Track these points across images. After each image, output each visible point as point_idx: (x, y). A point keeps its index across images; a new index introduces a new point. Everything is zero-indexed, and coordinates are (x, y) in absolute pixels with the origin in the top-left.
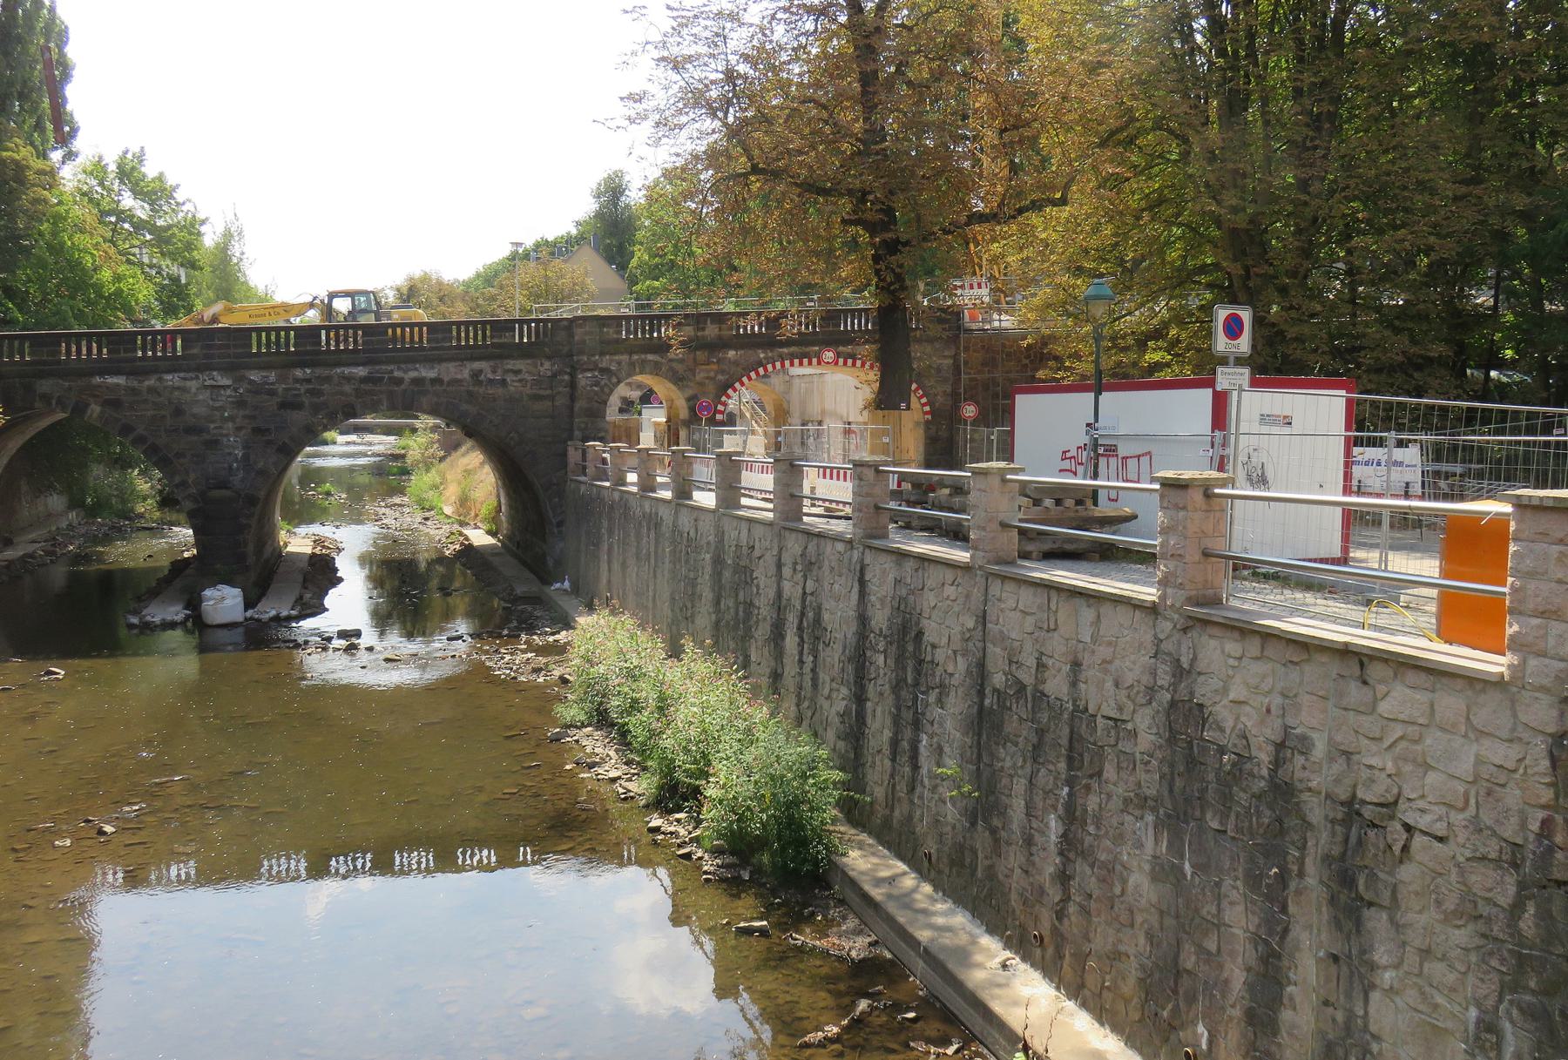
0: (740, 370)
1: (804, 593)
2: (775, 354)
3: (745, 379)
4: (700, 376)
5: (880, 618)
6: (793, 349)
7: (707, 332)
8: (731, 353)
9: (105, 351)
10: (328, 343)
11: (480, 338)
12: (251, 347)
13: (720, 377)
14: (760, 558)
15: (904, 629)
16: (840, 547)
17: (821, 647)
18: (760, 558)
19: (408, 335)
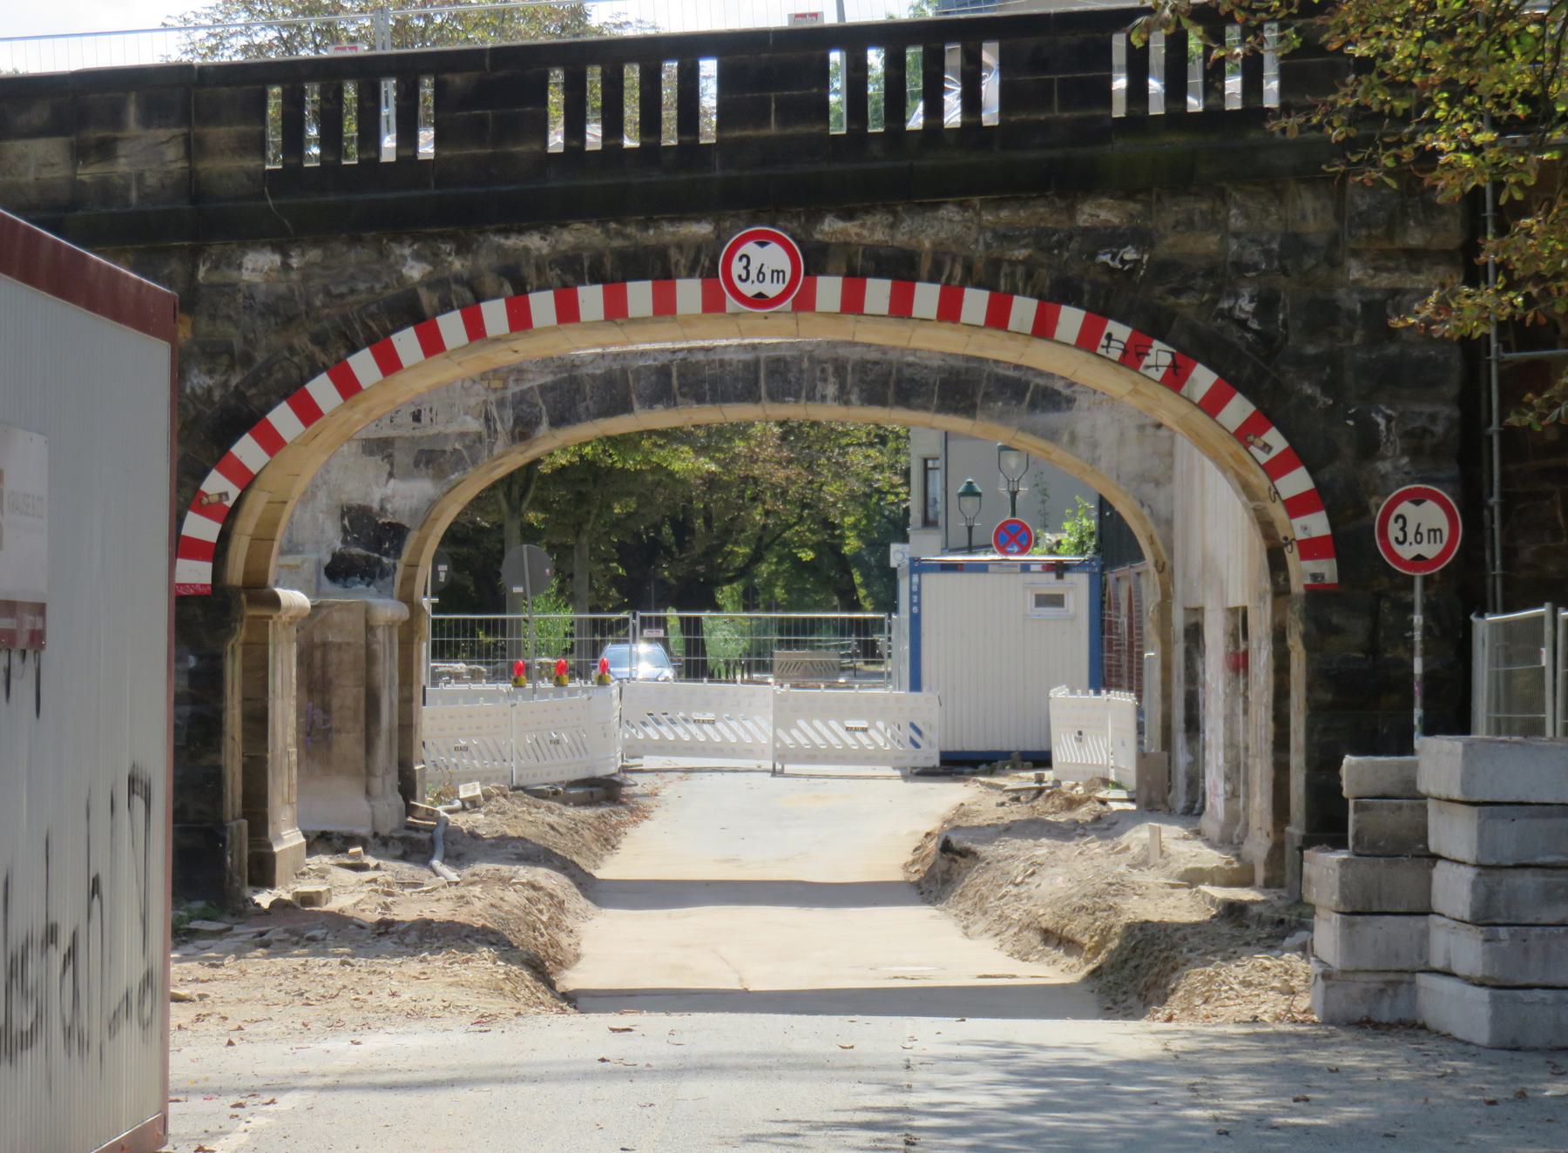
0: (302, 341)
2: (485, 261)
3: (321, 389)
6: (570, 237)
7: (122, 166)
10: (1138, 91)
11: (632, 111)
12: (543, 134)
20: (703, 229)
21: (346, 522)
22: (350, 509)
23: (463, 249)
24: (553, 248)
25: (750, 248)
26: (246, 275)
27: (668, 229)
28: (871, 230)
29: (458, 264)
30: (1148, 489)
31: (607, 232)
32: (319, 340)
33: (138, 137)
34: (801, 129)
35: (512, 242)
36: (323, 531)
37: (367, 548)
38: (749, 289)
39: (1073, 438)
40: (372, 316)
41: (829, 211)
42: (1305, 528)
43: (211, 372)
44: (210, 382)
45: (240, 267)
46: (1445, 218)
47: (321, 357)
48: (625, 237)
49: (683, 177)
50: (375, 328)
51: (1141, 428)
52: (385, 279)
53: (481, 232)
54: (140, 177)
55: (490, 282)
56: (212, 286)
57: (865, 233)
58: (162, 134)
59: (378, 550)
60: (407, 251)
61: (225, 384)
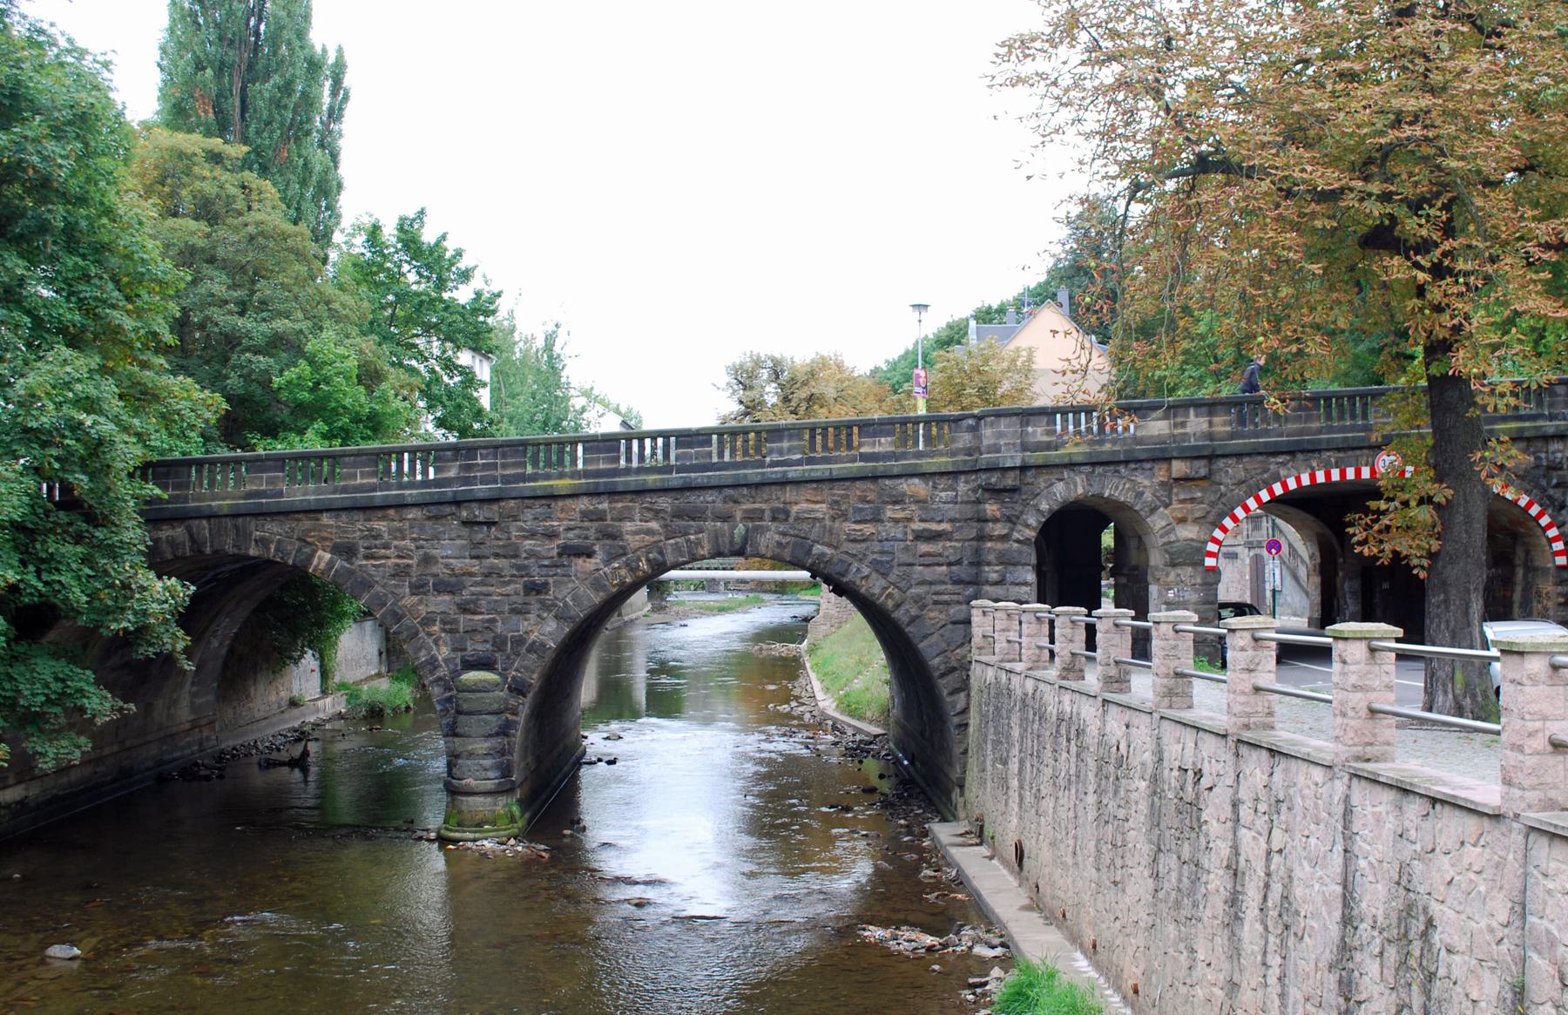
1: (1269, 853)
5: (1375, 900)
9: (431, 470)
14: (1210, 789)
15: (1409, 910)
16: (1318, 774)
17: (1291, 941)
18: (1210, 789)
19: (648, 451)
58: (1202, 420)
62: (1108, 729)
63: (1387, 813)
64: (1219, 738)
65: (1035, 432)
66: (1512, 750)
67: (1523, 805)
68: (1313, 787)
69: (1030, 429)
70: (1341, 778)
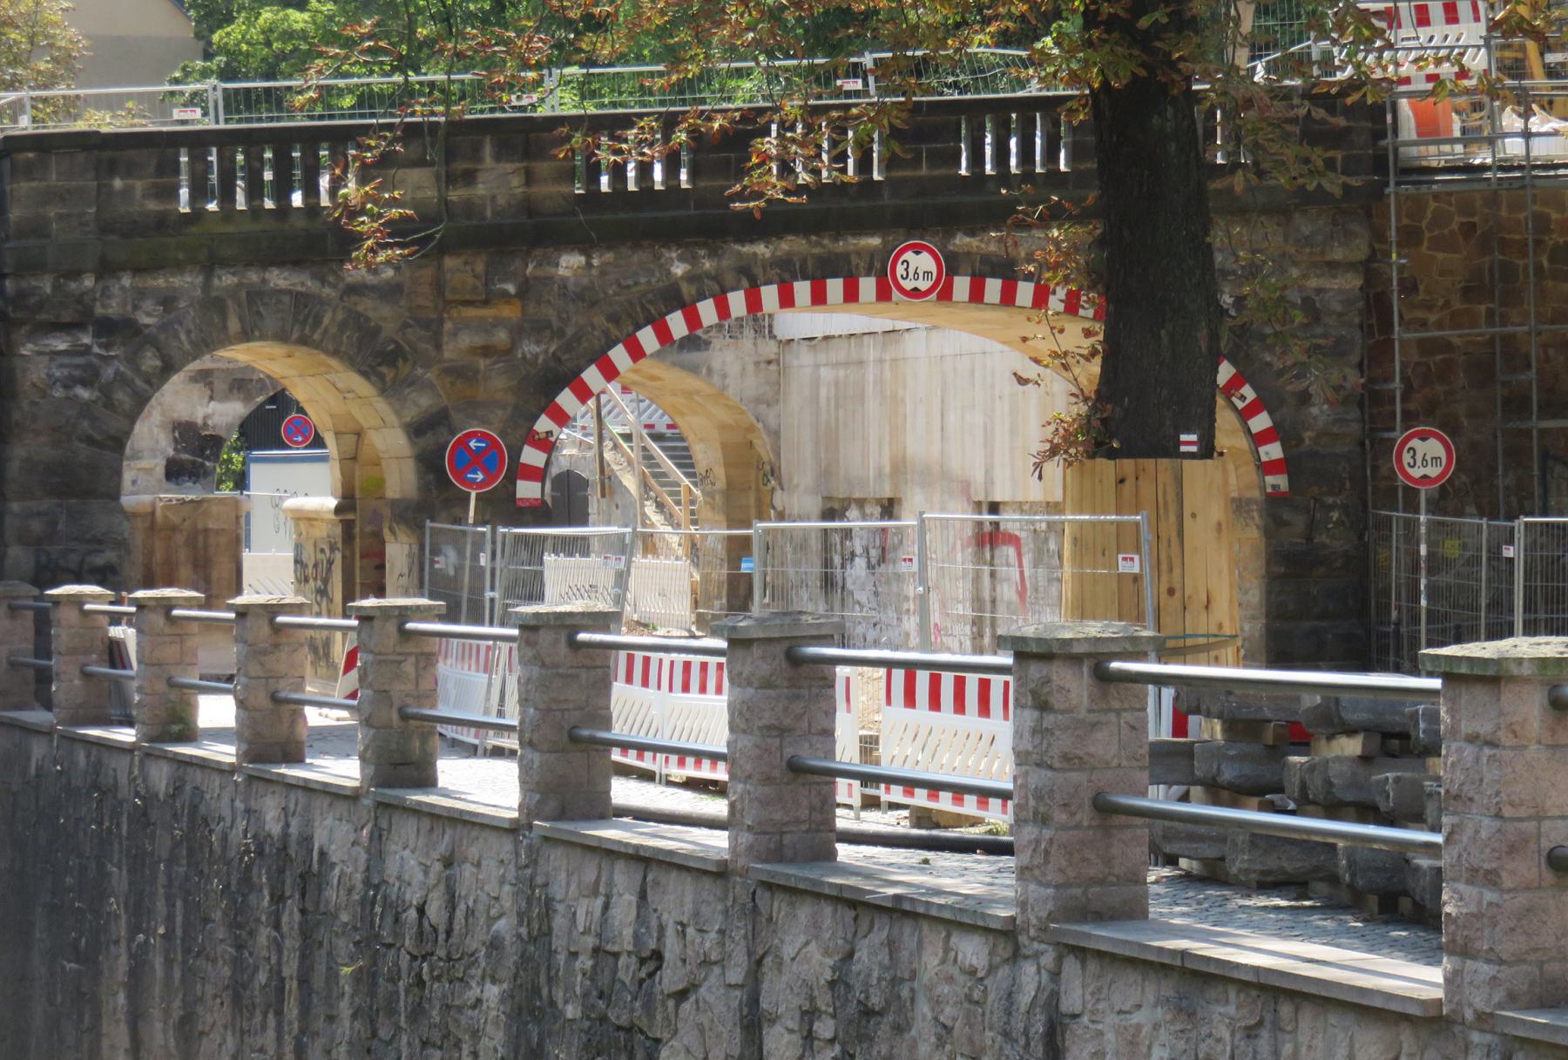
0: (600, 320)
3: (619, 355)
4: (458, 345)
7: (481, 190)
8: (570, 263)
13: (529, 348)
16: (972, 950)
20: (875, 241)
21: (177, 434)
22: (180, 424)
23: (713, 253)
24: (773, 254)
25: (909, 256)
26: (561, 271)
27: (852, 241)
28: (989, 242)
29: (707, 265)
30: (763, 408)
31: (810, 242)
32: (615, 319)
33: (492, 169)
34: (941, 172)
35: (747, 249)
36: (157, 442)
37: (193, 454)
38: (908, 285)
39: (710, 371)
40: (650, 302)
41: (959, 230)
42: (1267, 453)
43: (538, 343)
44: (538, 350)
45: (557, 265)
46: (1358, 241)
47: (615, 332)
48: (823, 246)
49: (863, 204)
50: (653, 311)
51: (757, 364)
52: (657, 274)
53: (725, 242)
54: (494, 198)
55: (729, 279)
56: (535, 278)
57: (983, 246)
58: (509, 167)
59: (201, 455)
60: (674, 255)
61: (546, 351)
62: (392, 869)
63: (1156, 1027)
64: (707, 883)
65: (127, 192)
66: (1470, 882)
67: (1499, 996)
68: (961, 978)
69: (118, 183)
70: (1037, 956)
